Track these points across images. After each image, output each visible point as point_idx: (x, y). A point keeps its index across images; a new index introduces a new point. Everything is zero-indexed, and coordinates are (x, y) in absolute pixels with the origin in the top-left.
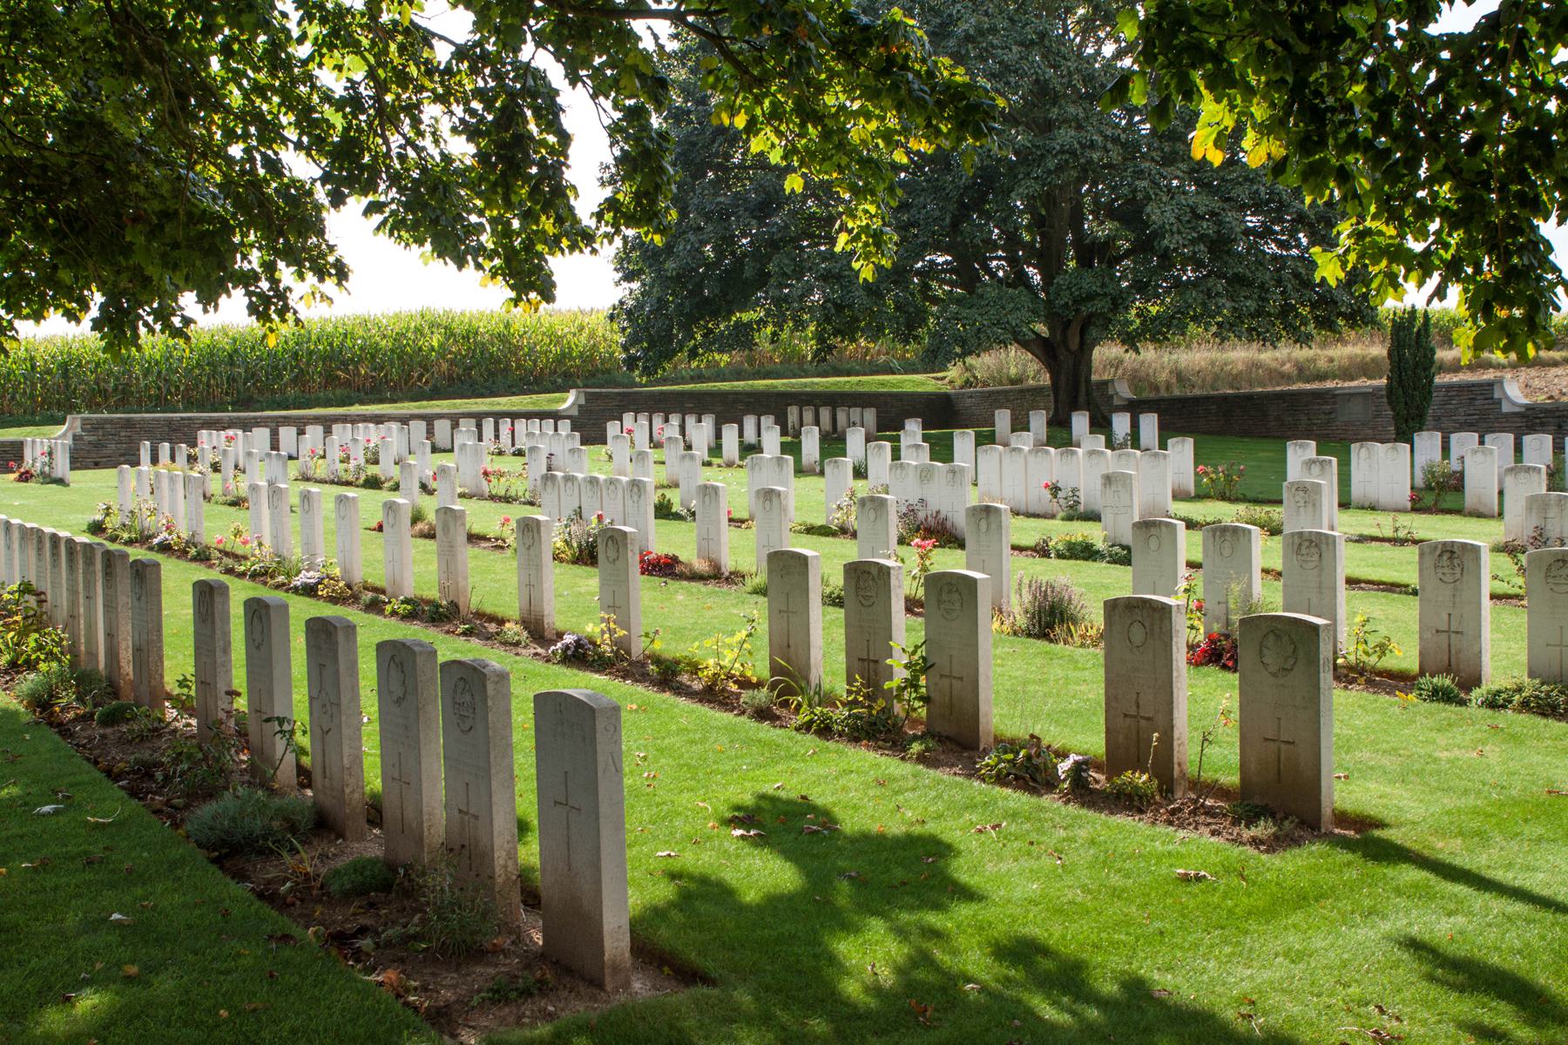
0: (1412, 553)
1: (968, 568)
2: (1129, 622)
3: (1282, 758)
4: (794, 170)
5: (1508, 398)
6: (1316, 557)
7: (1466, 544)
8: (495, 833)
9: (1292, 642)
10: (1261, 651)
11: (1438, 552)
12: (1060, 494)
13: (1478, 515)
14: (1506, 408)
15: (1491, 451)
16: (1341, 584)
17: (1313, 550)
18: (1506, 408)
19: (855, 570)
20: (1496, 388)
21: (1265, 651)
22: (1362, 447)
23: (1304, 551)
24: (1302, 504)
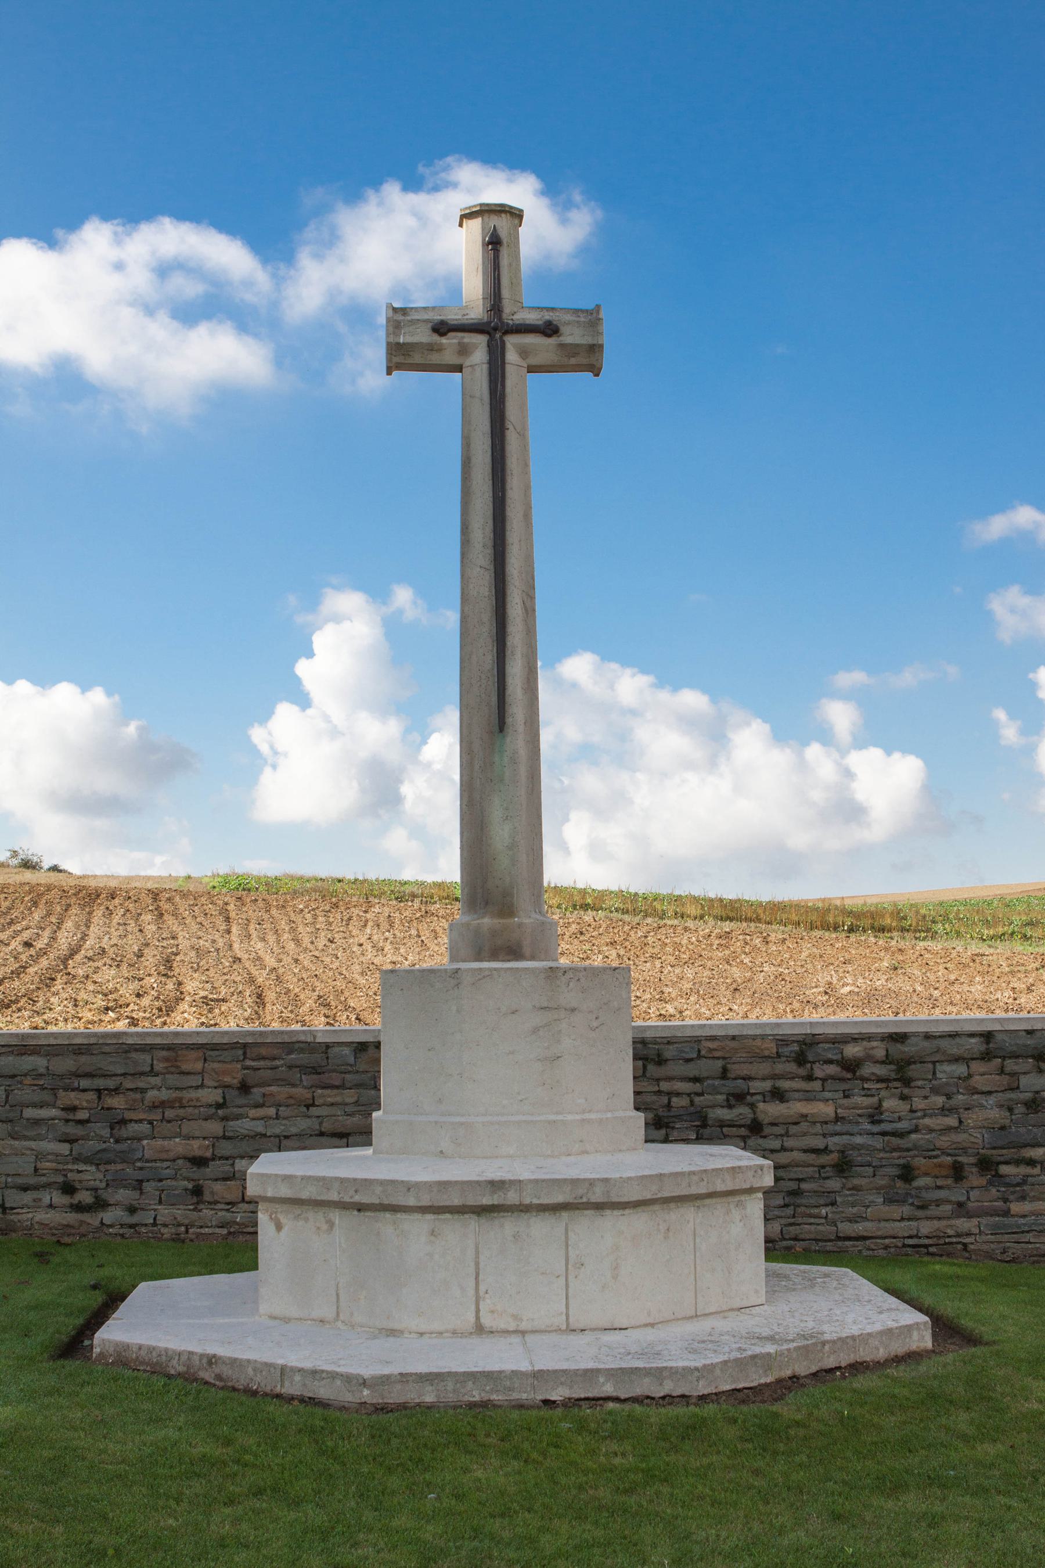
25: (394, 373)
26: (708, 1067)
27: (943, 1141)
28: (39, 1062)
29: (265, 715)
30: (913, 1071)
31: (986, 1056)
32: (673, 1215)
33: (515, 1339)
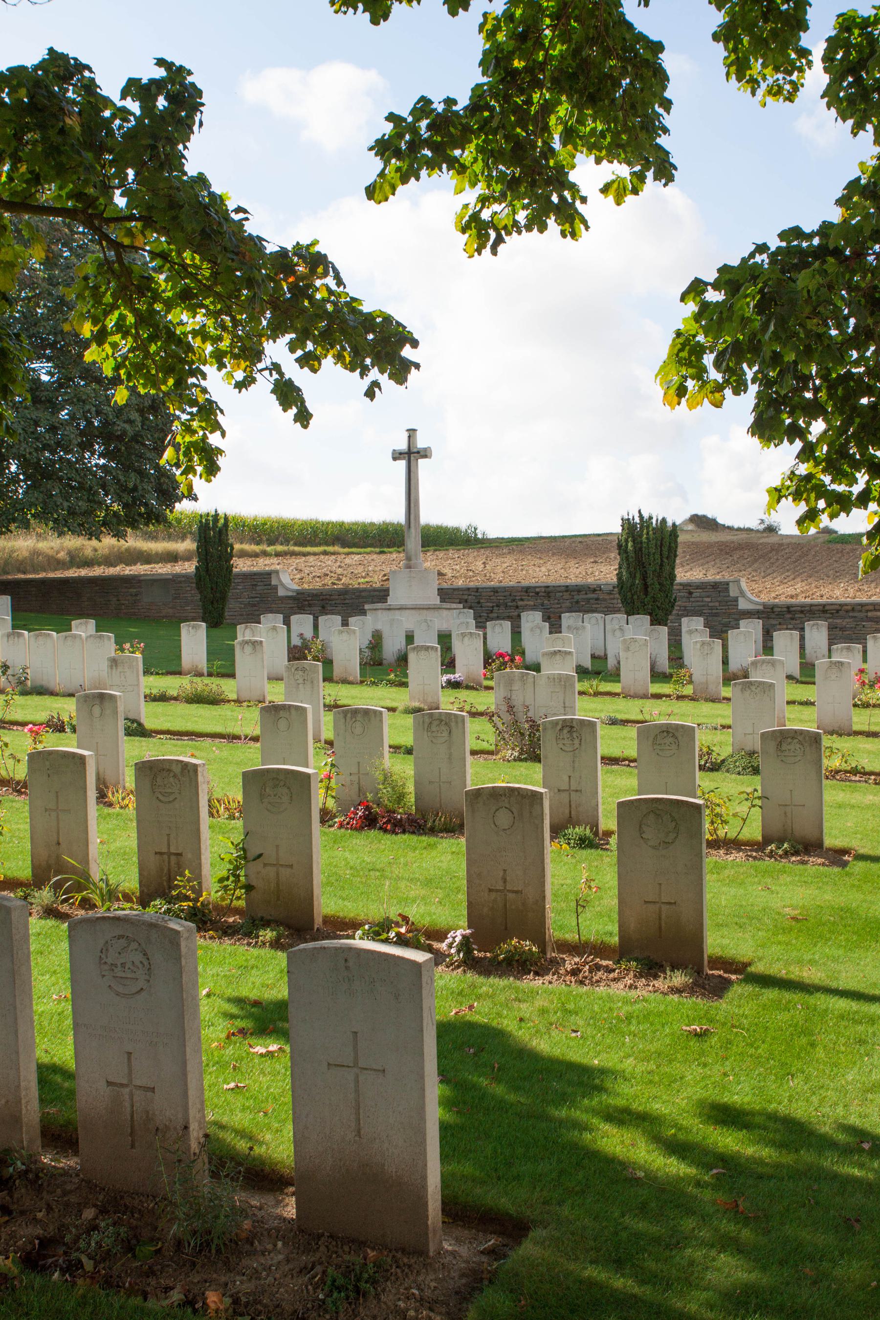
0: (632, 732)
1: (78, 747)
2: (494, 808)
3: (663, 916)
4: (121, 382)
5: (282, 584)
6: (445, 734)
7: (583, 720)
8: (190, 1104)
9: (673, 819)
10: (640, 826)
11: (559, 727)
12: (9, 672)
13: (345, 681)
14: (281, 593)
15: (354, 632)
16: (468, 754)
17: (443, 728)
18: (281, 593)
19: (151, 768)
20: (273, 576)
21: (645, 828)
22: (246, 627)
23: (434, 728)
24: (301, 681)
25: (827, 76)
26: (507, 594)
27: (557, 610)
28: (377, 593)
29: (799, 39)
30: (551, 594)
31: (567, 591)
32: (421, 611)
33: (485, 719)
